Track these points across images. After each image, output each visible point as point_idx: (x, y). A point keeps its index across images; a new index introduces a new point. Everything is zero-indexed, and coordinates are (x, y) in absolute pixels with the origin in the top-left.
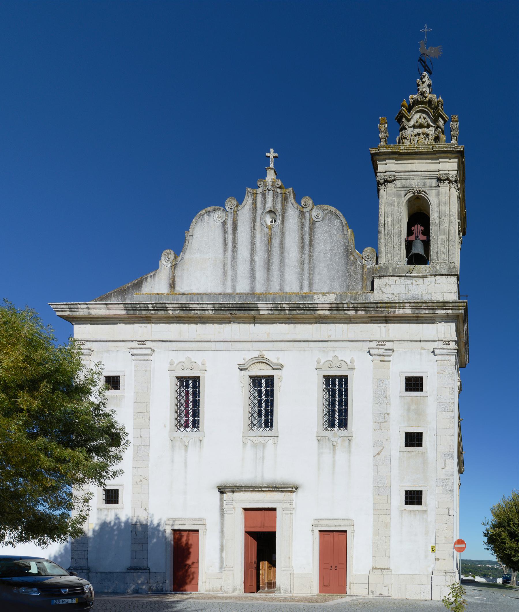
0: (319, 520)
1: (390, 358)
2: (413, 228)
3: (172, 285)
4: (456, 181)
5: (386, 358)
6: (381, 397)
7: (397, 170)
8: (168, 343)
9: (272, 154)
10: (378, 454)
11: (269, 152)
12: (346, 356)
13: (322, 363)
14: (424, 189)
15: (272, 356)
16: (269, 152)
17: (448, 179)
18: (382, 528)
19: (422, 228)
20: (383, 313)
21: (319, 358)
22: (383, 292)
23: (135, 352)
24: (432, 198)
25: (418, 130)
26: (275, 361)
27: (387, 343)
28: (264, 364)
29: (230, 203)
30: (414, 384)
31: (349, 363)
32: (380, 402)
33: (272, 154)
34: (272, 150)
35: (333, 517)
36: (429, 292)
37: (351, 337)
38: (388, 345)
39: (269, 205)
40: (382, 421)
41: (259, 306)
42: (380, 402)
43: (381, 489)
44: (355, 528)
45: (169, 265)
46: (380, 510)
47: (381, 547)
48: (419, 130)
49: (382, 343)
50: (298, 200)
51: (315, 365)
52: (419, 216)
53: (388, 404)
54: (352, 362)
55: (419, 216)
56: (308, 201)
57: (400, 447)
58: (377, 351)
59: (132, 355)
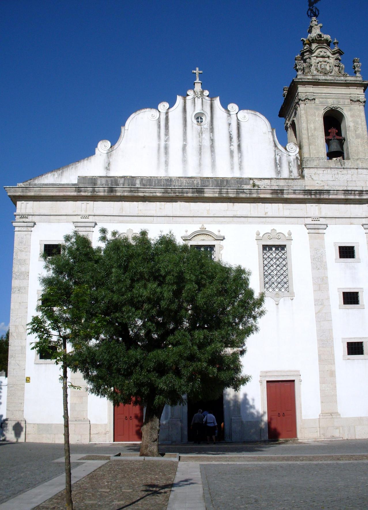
0: (266, 372)
1: (324, 231)
2: (329, 131)
3: (108, 168)
4: (364, 102)
5: (320, 231)
6: (318, 262)
7: (315, 92)
8: (109, 217)
9: (197, 71)
10: (319, 312)
11: (195, 70)
12: (282, 228)
13: (261, 235)
14: (339, 106)
15: (213, 228)
16: (195, 70)
17: (359, 101)
18: (328, 376)
19: (337, 131)
20: (317, 197)
21: (258, 231)
22: (312, 179)
23: (79, 224)
24: (346, 113)
25: (323, 61)
26: (216, 233)
27: (321, 219)
28: (200, 236)
29: (163, 106)
30: (347, 252)
31: (287, 235)
32: (318, 267)
33: (197, 71)
34: (197, 69)
35: (280, 370)
36: (353, 180)
37: (287, 214)
38: (322, 221)
39: (198, 109)
40: (321, 283)
41: (205, 190)
42: (318, 267)
43: (325, 342)
44: (302, 378)
45: (106, 152)
46: (325, 359)
47: (328, 396)
48: (321, 59)
49: (317, 219)
50: (225, 105)
51: (255, 236)
52: (333, 121)
53: (325, 268)
54: (290, 234)
55: (333, 121)
56: (233, 107)
57: (340, 305)
58: (313, 226)
59: (76, 227)
